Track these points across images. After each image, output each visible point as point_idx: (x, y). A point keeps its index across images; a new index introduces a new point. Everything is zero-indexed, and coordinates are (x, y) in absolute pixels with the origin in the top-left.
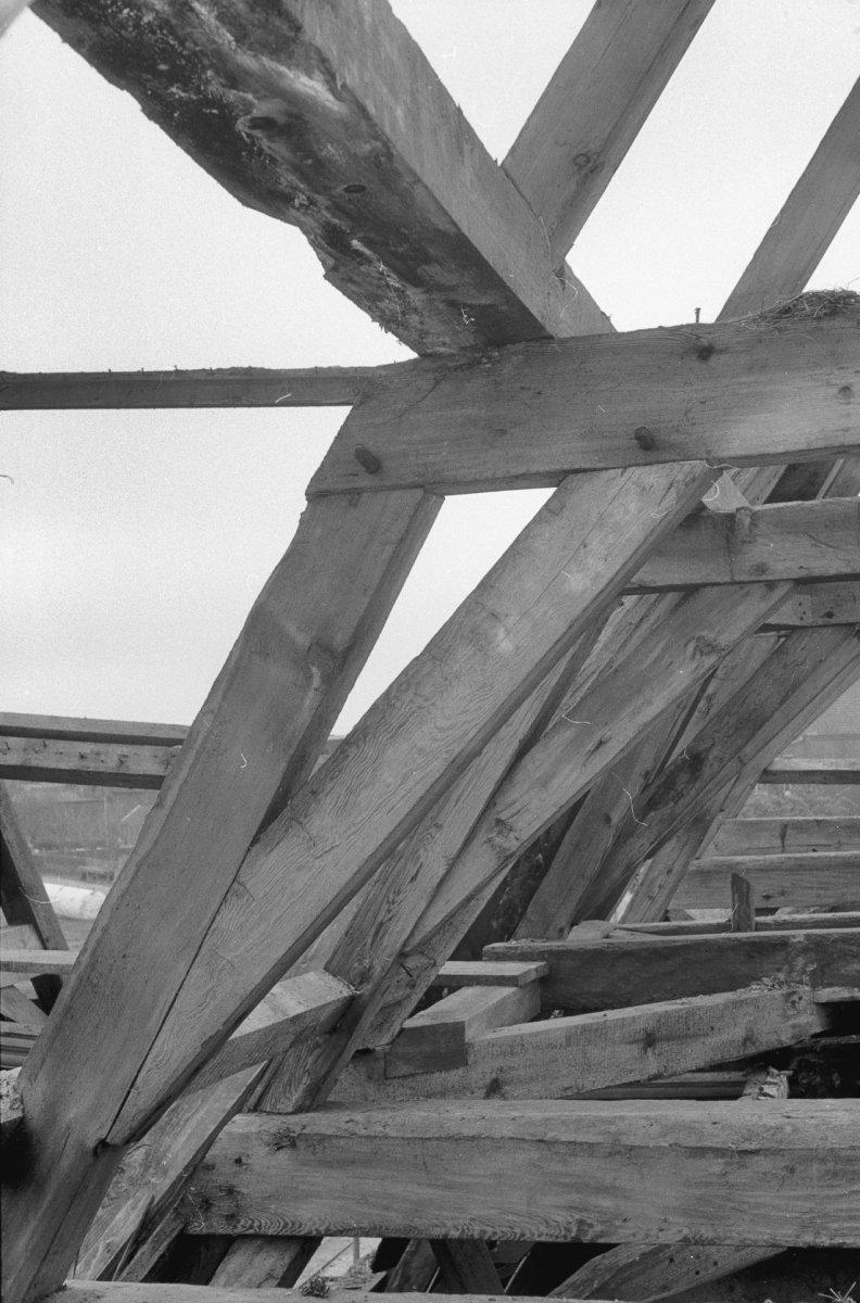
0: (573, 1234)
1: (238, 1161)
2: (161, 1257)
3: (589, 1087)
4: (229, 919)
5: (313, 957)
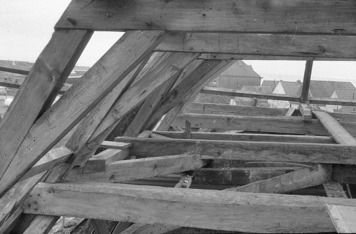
0: (126, 220)
1: (39, 195)
2: (17, 219)
3: (138, 178)
4: (26, 143)
5: (65, 140)
